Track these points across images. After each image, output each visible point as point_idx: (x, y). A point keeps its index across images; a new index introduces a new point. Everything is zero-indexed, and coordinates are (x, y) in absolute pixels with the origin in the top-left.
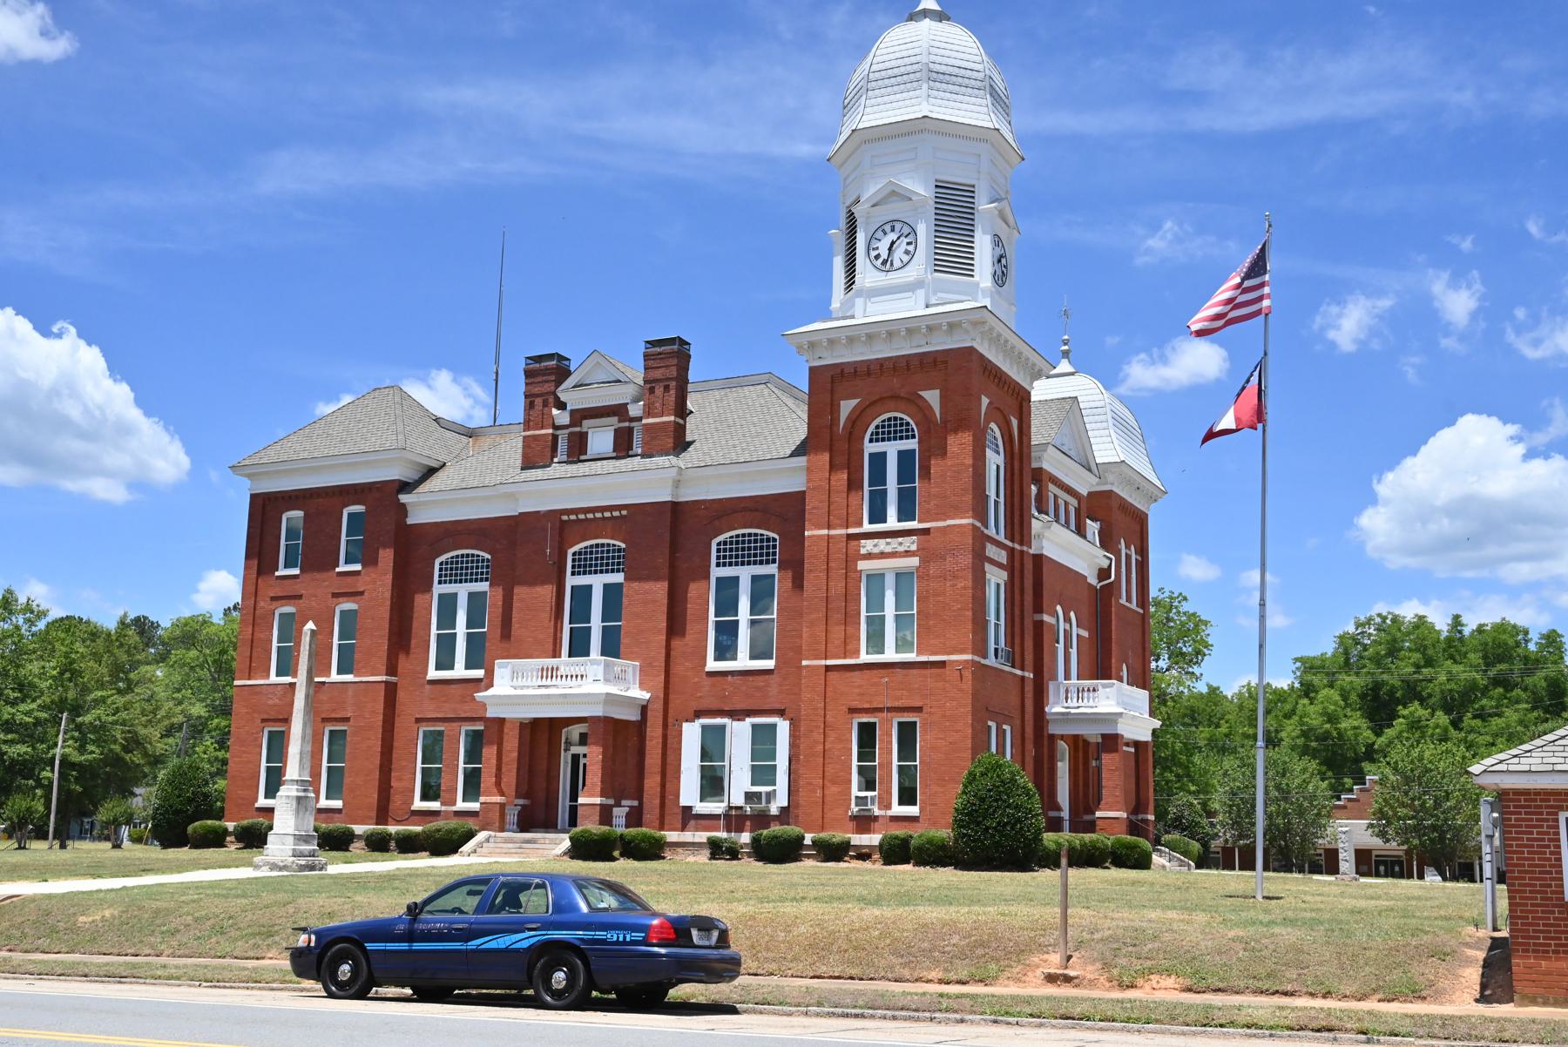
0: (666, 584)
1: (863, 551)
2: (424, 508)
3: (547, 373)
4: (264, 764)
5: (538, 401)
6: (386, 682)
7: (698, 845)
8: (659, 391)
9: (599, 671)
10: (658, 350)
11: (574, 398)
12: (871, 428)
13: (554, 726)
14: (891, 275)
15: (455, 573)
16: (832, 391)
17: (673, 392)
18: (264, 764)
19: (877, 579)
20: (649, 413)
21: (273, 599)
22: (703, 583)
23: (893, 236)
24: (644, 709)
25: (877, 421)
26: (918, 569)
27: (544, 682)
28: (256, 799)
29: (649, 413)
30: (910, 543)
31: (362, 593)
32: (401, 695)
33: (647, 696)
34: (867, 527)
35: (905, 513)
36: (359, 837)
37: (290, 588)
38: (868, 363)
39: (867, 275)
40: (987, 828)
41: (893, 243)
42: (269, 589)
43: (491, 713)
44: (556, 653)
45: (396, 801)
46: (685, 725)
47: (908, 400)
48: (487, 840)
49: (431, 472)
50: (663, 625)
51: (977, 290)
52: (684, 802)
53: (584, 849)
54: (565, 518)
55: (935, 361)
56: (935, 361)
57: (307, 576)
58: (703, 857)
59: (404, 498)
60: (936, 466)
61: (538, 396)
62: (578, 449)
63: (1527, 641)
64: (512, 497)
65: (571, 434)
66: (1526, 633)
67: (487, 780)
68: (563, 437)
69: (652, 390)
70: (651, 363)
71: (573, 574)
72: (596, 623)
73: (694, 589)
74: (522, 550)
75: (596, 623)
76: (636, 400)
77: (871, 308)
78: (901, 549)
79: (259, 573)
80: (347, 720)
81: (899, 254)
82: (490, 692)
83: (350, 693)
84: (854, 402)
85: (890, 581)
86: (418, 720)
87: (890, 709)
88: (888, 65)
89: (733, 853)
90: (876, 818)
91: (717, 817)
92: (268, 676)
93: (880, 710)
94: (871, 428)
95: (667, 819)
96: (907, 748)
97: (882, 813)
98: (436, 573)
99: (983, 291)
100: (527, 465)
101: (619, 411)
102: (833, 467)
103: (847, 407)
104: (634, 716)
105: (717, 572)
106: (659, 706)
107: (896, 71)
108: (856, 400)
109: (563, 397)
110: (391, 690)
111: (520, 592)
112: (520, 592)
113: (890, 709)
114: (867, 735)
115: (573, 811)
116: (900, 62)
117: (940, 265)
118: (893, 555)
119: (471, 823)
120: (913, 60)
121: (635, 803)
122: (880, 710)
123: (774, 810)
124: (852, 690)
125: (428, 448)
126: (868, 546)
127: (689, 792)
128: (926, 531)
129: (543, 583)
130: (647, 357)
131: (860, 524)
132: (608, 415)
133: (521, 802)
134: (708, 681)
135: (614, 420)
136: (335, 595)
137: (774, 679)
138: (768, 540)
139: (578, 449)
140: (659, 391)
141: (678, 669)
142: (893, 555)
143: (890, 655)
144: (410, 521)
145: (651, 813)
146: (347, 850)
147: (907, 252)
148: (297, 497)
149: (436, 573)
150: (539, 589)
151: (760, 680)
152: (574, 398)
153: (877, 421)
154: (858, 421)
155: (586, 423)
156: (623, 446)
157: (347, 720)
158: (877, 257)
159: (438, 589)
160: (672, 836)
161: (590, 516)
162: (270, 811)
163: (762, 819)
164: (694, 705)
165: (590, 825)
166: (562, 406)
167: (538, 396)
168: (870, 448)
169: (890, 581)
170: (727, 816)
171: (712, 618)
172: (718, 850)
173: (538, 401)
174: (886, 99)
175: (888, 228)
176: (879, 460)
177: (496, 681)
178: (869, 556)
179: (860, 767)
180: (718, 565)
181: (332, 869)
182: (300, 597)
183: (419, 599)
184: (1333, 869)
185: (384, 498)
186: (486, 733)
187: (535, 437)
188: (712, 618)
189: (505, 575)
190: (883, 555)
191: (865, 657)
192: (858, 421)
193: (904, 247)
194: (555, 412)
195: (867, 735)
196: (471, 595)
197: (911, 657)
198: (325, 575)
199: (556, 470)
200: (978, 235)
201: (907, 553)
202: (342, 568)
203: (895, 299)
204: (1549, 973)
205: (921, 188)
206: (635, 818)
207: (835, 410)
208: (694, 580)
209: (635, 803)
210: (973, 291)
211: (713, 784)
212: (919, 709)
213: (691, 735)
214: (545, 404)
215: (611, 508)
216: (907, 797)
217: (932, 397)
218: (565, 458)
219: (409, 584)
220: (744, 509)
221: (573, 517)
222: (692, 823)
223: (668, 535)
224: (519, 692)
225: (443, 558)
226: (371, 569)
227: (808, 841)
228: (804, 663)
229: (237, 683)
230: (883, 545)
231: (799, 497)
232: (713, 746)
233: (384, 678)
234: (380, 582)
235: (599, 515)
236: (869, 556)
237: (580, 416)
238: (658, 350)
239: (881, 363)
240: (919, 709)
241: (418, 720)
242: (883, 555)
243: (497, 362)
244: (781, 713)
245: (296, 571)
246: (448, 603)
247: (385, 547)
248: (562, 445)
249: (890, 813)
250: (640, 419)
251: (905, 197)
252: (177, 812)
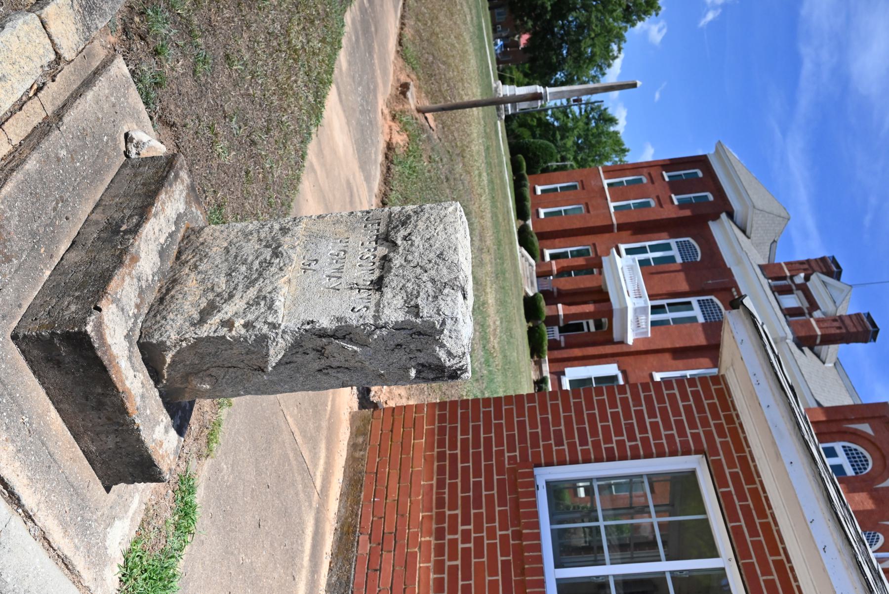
2: (722, 231)
3: (830, 268)
6: (613, 225)
8: (836, 324)
9: (641, 303)
10: (865, 320)
12: (853, 446)
15: (681, 247)
16: (873, 418)
17: (838, 331)
20: (818, 321)
21: (650, 174)
25: (860, 449)
28: (539, 185)
29: (818, 321)
32: (607, 235)
33: (630, 341)
43: (605, 259)
45: (548, 242)
48: (530, 265)
49: (744, 231)
50: (679, 344)
52: (567, 370)
54: (734, 290)
58: (534, 376)
59: (724, 216)
62: (781, 291)
64: (739, 262)
65: (790, 286)
67: (564, 263)
68: (788, 282)
70: (854, 319)
71: (699, 301)
72: (669, 316)
75: (669, 316)
76: (824, 313)
86: (594, 245)
94: (853, 446)
104: (616, 336)
106: (624, 349)
109: (813, 277)
110: (607, 229)
112: (682, 276)
119: (539, 257)
121: (563, 344)
125: (756, 223)
130: (858, 315)
133: (555, 290)
134: (646, 374)
135: (806, 305)
136: (658, 197)
139: (781, 291)
140: (836, 324)
141: (651, 358)
144: (712, 225)
145: (557, 354)
152: (816, 283)
153: (860, 449)
154: (856, 437)
155: (800, 293)
156: (789, 313)
159: (673, 242)
164: (629, 370)
165: (546, 310)
166: (807, 278)
173: (806, 266)
181: (499, 123)
182: (661, 206)
183: (665, 234)
184: (612, 231)
186: (594, 265)
192: (856, 437)
194: (802, 275)
199: (765, 282)
204: (404, 447)
206: (554, 345)
209: (563, 344)
222: (556, 377)
237: (804, 289)
238: (865, 320)
241: (594, 245)
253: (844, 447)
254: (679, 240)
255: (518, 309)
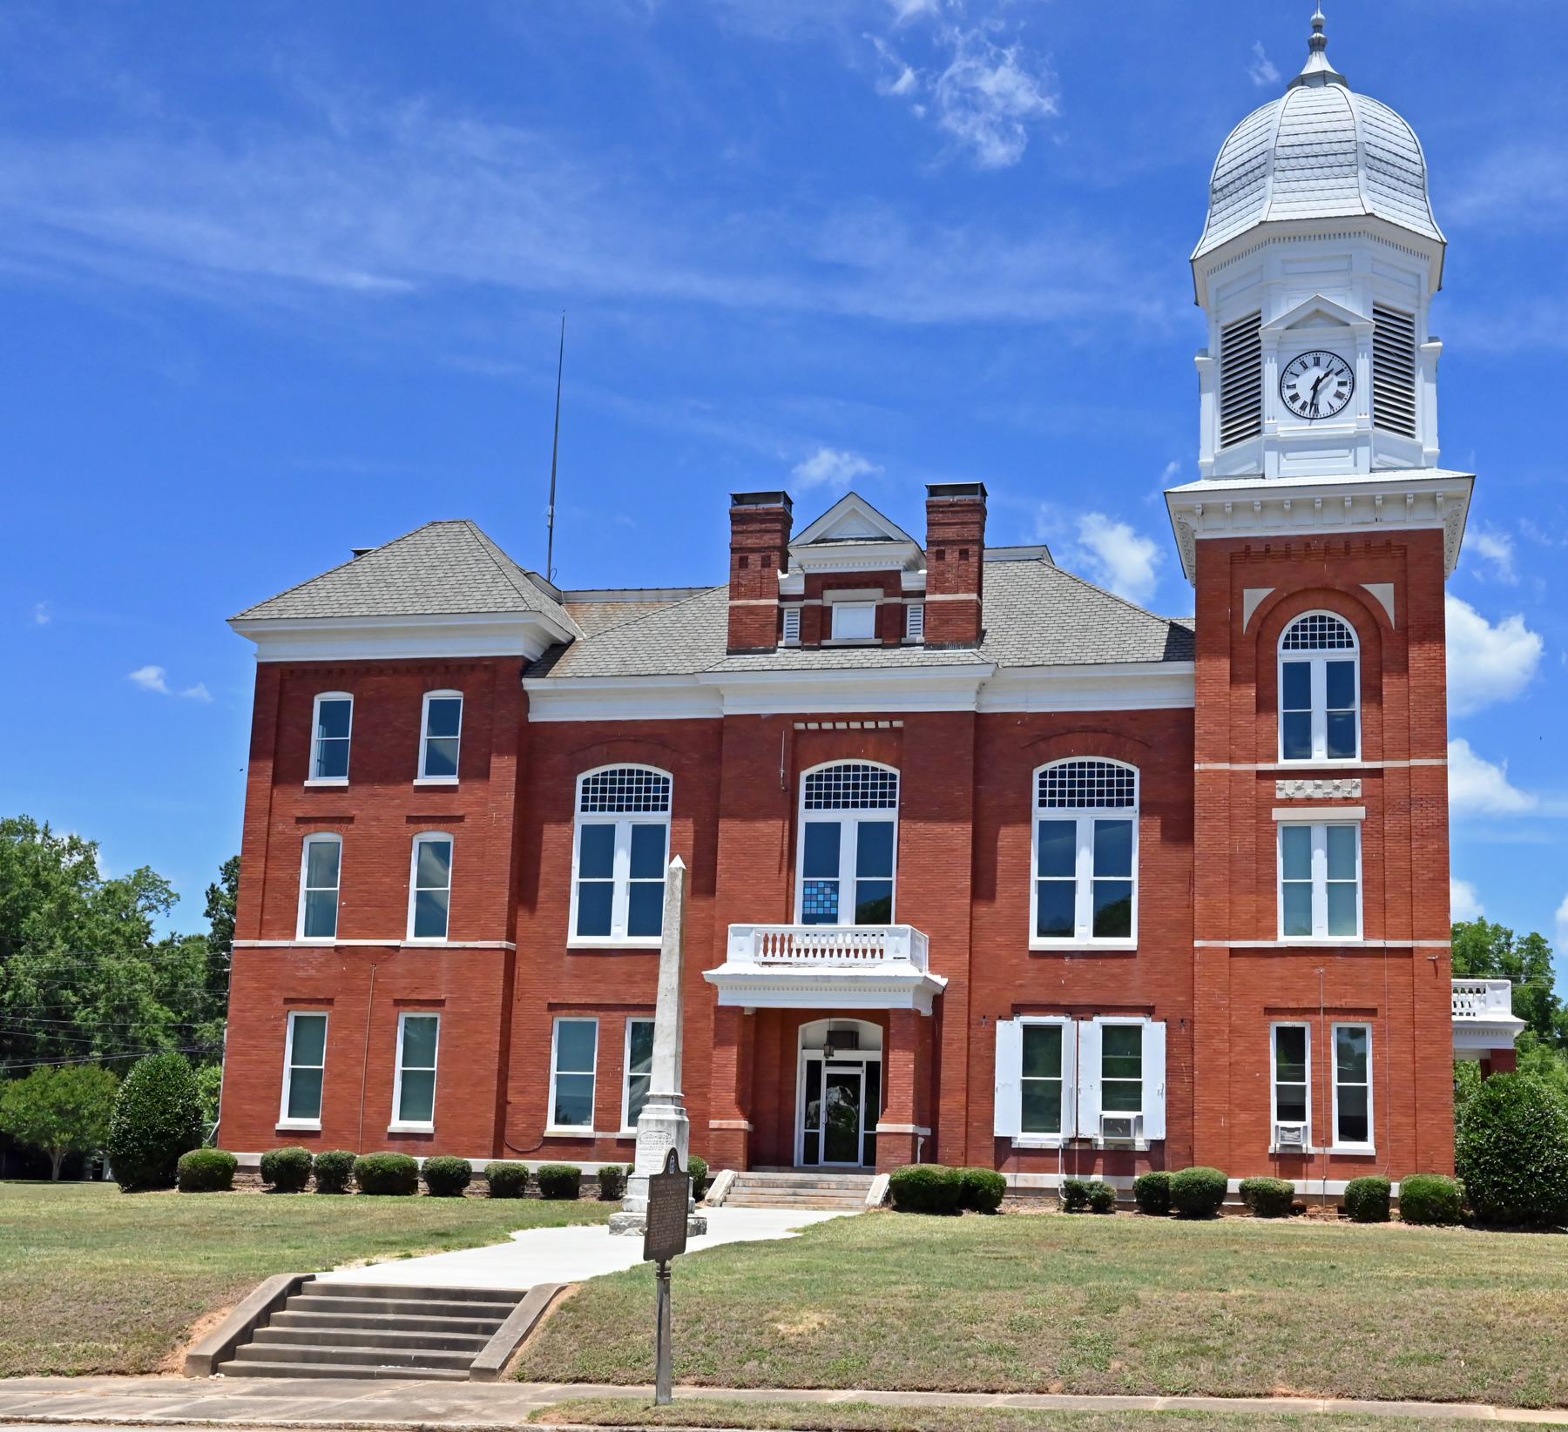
0: (969, 827)
1: (1280, 795)
2: (553, 701)
3: (762, 524)
4: (288, 1065)
5: (754, 559)
6: (506, 950)
7: (1051, 1193)
8: (952, 556)
11: (806, 559)
12: (1287, 630)
13: (787, 1021)
14: (1316, 425)
18: (288, 1065)
19: (1300, 835)
20: (936, 583)
21: (299, 820)
22: (1020, 829)
23: (1317, 372)
24: (938, 1000)
26: (1363, 823)
27: (769, 958)
28: (277, 1119)
30: (1353, 788)
31: (461, 819)
32: (522, 969)
34: (1283, 763)
35: (1340, 742)
36: (590, 1179)
37: (328, 806)
38: (1287, 541)
39: (1278, 421)
40: (1533, 1175)
41: (1319, 381)
42: (292, 804)
44: (788, 920)
45: (518, 1123)
46: (1000, 1024)
47: (1346, 594)
51: (1421, 458)
52: (999, 1131)
53: (905, 1197)
54: (800, 726)
55: (1388, 544)
56: (1388, 544)
57: (362, 790)
60: (1391, 686)
61: (753, 550)
62: (816, 630)
63: (1509, 945)
64: (718, 693)
66: (1509, 936)
69: (940, 556)
70: (938, 517)
73: (1006, 836)
74: (725, 773)
76: (912, 566)
77: (1286, 466)
78: (1338, 795)
79: (276, 781)
80: (439, 1003)
81: (1326, 397)
82: (723, 970)
83: (444, 964)
84: (1265, 592)
85: (1319, 837)
86: (552, 1007)
87: (1328, 1011)
88: (1302, 139)
89: (1102, 1205)
90: (1309, 1158)
91: (1052, 1153)
92: (293, 935)
93: (1315, 1011)
94: (1287, 630)
95: (971, 1153)
96: (1352, 1065)
97: (1320, 1150)
98: (579, 795)
99: (1427, 456)
100: (737, 647)
101: (887, 581)
102: (1234, 679)
103: (1253, 598)
105: (1040, 814)
107: (1317, 149)
108: (1251, 591)
111: (729, 829)
113: (1328, 1011)
114: (1291, 1043)
115: (871, 1141)
116: (1321, 137)
117: (1381, 419)
118: (1326, 802)
120: (1341, 136)
122: (1315, 1011)
123: (1140, 1144)
124: (1274, 982)
126: (1287, 788)
127: (1007, 1119)
128: (1378, 773)
129: (767, 817)
130: (931, 508)
131: (1275, 759)
132: (867, 585)
134: (569, 959)
135: (877, 594)
137: (1138, 963)
138: (884, 776)
139: (816, 630)
142: (1326, 802)
143: (1320, 936)
146: (460, 1195)
147: (1339, 395)
148: (342, 671)
149: (579, 795)
150: (761, 826)
151: (1114, 966)
152: (806, 559)
155: (830, 596)
156: (890, 629)
157: (439, 1003)
158: (1294, 398)
159: (581, 819)
160: (1011, 1179)
161: (841, 725)
162: (630, 1143)
163: (1120, 1159)
164: (1013, 997)
167: (753, 550)
168: (1285, 656)
169: (1319, 837)
170: (1067, 1152)
171: (1035, 876)
172: (1075, 1199)
174: (1303, 184)
175: (1309, 360)
176: (1299, 674)
177: (730, 955)
178: (1289, 802)
179: (1339, 1088)
180: (808, 806)
182: (351, 820)
183: (550, 832)
185: (495, 684)
187: (751, 610)
188: (1035, 876)
189: (705, 808)
190: (1309, 802)
191: (1283, 940)
192: (1269, 617)
193: (1334, 387)
195: (1291, 1043)
196: (863, 828)
197: (1357, 939)
198: (391, 790)
199: (781, 657)
200: (1419, 380)
201: (1347, 801)
202: (422, 780)
203: (1320, 457)
205: (1359, 311)
207: (1237, 602)
208: (1007, 823)
210: (1415, 457)
211: (1041, 1106)
212: (1371, 1012)
213: (1009, 1037)
214: (766, 563)
215: (862, 717)
216: (1353, 1128)
217: (1383, 593)
218: (796, 641)
219: (539, 806)
220: (1085, 729)
221: (813, 726)
222: (1012, 1160)
223: (970, 758)
224: (767, 971)
225: (590, 774)
226: (476, 785)
227: (1234, 1185)
228: (1197, 944)
229: (236, 943)
230: (1309, 788)
231: (1184, 719)
232: (1042, 1050)
233: (504, 944)
234: (496, 800)
235: (855, 725)
236: (1289, 802)
237: (818, 583)
239: (1307, 542)
240: (1371, 1012)
241: (552, 1007)
242: (1309, 802)
243: (552, 503)
244: (1149, 1011)
245: (343, 781)
246: (599, 845)
247: (501, 753)
248: (792, 624)
249: (618, 1135)
250: (922, 594)
251: (1342, 322)
252: (162, 1136)
253: (1286, 646)
254: (1036, 798)
255: (1497, 1239)
